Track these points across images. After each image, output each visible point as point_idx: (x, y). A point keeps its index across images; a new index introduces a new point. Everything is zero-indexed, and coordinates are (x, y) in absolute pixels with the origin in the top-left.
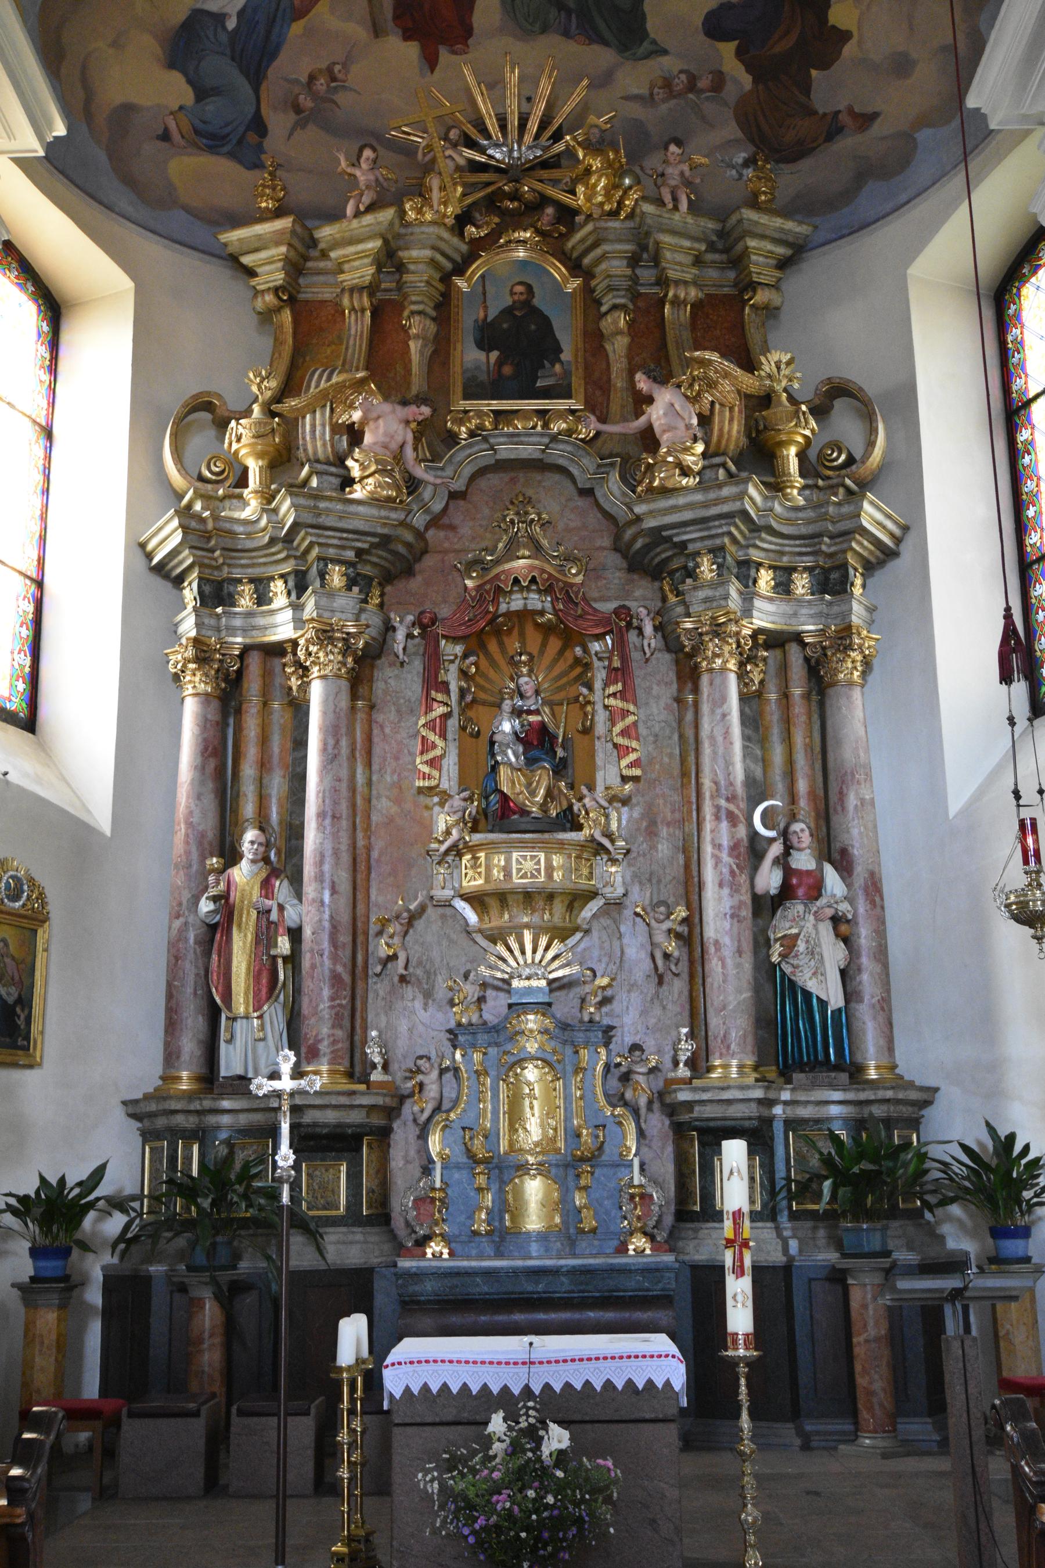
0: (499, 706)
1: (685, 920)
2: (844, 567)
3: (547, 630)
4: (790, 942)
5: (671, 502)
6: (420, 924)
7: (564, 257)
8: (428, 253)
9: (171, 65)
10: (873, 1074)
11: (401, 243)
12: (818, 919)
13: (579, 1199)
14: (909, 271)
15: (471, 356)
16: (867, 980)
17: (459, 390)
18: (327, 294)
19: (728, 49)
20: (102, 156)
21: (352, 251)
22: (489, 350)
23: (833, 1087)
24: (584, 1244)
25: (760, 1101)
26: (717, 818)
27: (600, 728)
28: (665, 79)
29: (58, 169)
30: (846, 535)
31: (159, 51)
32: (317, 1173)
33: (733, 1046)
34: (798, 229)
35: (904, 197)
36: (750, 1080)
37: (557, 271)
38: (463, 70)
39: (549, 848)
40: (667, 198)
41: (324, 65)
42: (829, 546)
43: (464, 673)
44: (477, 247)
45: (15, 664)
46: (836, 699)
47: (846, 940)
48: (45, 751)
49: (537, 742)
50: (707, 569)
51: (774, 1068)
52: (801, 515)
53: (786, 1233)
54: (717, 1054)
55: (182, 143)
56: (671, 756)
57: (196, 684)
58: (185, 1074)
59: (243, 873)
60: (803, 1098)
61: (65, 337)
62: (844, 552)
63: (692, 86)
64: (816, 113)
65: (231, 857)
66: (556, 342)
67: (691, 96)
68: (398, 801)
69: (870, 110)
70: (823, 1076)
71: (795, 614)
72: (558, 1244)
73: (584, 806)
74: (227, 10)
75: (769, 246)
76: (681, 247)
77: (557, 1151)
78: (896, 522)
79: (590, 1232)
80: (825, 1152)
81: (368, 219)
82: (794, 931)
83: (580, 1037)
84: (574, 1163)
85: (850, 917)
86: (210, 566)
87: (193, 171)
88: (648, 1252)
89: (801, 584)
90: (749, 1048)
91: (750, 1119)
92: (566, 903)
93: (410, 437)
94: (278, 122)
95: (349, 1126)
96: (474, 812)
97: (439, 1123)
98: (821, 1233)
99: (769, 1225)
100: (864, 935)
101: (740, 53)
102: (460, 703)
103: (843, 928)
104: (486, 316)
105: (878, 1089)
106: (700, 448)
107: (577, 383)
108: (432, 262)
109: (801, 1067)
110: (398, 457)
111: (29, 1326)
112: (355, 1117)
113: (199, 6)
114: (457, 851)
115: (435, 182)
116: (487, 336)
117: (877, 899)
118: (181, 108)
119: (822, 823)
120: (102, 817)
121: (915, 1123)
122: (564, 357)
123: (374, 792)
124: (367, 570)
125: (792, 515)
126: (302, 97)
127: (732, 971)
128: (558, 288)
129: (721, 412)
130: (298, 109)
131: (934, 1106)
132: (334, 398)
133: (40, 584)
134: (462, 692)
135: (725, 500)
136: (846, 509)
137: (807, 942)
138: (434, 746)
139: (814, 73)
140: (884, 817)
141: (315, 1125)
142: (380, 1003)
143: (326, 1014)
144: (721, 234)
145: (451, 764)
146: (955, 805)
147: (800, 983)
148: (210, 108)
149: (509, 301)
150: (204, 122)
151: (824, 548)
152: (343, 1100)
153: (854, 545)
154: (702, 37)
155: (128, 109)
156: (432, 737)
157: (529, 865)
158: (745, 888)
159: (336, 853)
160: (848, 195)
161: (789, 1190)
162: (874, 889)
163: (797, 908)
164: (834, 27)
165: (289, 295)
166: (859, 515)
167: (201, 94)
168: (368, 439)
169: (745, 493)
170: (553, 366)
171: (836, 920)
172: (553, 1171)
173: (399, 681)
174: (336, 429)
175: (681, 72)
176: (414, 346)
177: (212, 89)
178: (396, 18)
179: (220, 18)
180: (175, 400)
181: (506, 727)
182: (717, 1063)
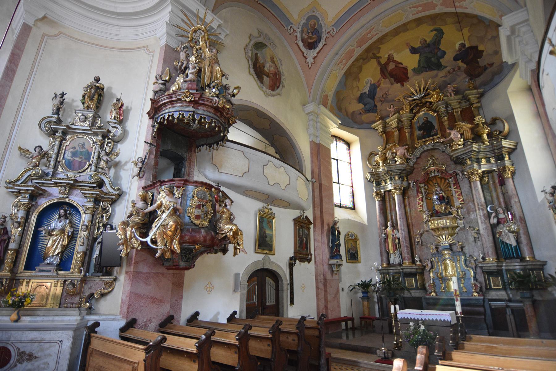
0: (433, 193)
2: (502, 154)
3: (441, 178)
6: (424, 235)
7: (432, 110)
10: (528, 259)
15: (417, 133)
16: (523, 239)
17: (416, 139)
18: (390, 130)
20: (351, 120)
21: (393, 122)
25: (497, 266)
26: (479, 210)
27: (454, 195)
36: (494, 262)
37: (431, 113)
38: (407, 85)
39: (448, 219)
40: (449, 94)
43: (425, 189)
44: (415, 114)
48: (357, 213)
49: (441, 199)
50: (469, 162)
57: (377, 199)
59: (389, 229)
61: (351, 148)
63: (454, 70)
65: (387, 227)
68: (416, 213)
70: (513, 260)
81: (394, 116)
83: (457, 254)
86: (375, 179)
87: (365, 117)
89: (493, 160)
93: (406, 151)
94: (378, 104)
101: (462, 62)
106: (462, 140)
107: (439, 132)
108: (407, 119)
110: (404, 155)
111: (363, 304)
112: (414, 270)
114: (428, 221)
115: (404, 107)
116: (420, 129)
120: (366, 222)
121: (542, 270)
124: (402, 175)
127: (487, 240)
128: (432, 116)
130: (381, 101)
132: (391, 148)
133: (352, 187)
134: (425, 192)
136: (498, 144)
143: (406, 253)
144: (463, 97)
145: (425, 206)
155: (354, 112)
157: (441, 223)
159: (403, 225)
160: (492, 79)
162: (523, 220)
165: (384, 132)
167: (365, 105)
168: (398, 154)
173: (413, 192)
174: (392, 153)
176: (407, 134)
179: (365, 93)
180: (368, 154)
181: (435, 197)
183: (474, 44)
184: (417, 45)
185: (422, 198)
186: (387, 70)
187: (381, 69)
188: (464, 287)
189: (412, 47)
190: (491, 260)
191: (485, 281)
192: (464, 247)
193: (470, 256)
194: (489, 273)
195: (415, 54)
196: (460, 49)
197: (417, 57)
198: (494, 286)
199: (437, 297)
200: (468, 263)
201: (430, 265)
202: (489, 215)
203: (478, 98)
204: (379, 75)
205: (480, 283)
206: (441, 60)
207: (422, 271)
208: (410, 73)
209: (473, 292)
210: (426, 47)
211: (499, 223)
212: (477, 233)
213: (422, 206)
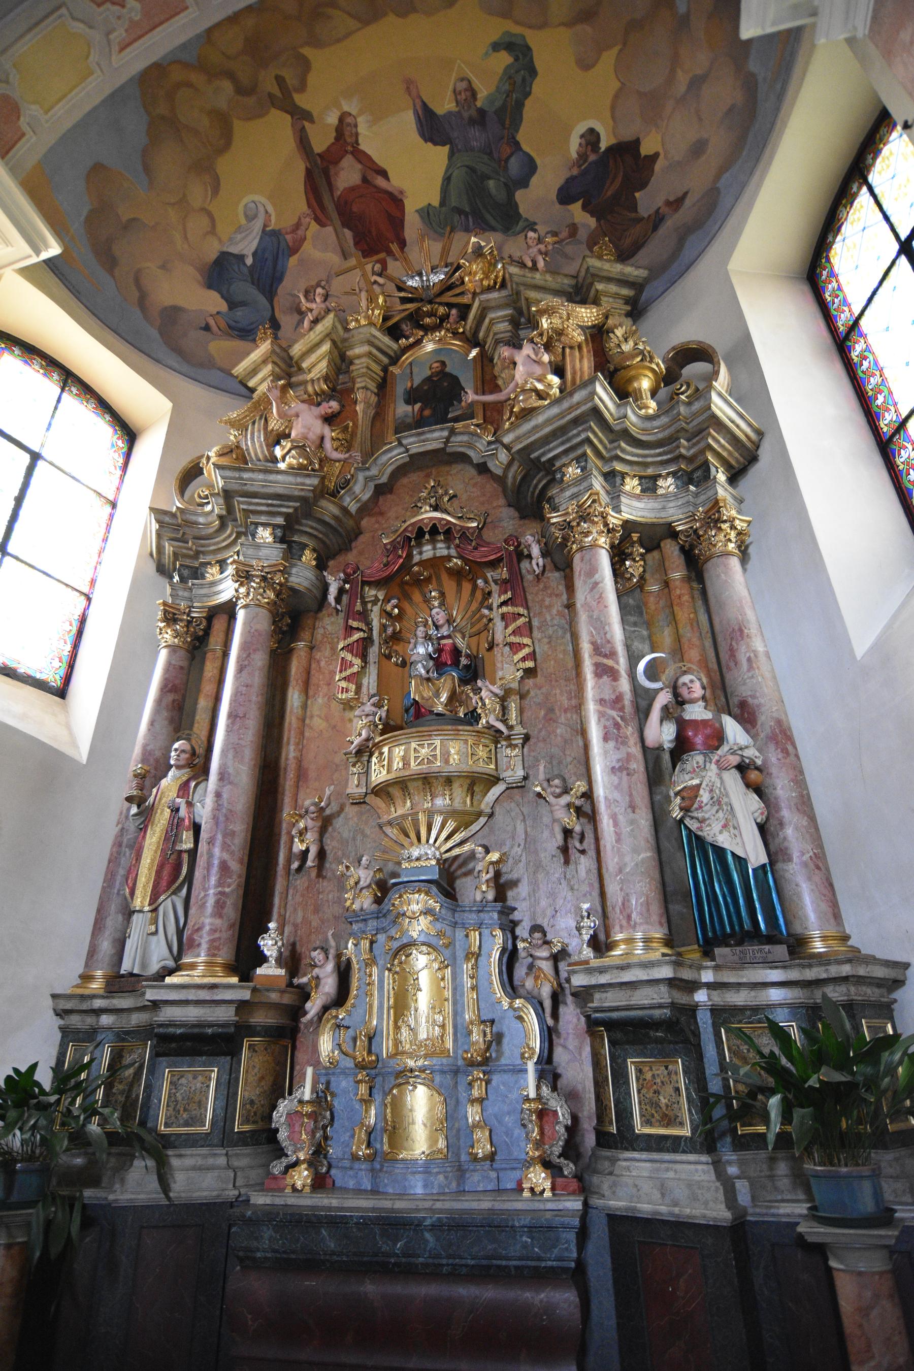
1: (584, 795)
4: (690, 795)
5: (533, 423)
8: (366, 348)
9: (210, 286)
10: (818, 947)
11: (347, 344)
12: (722, 768)
13: (473, 1114)
14: (729, 267)
16: (792, 834)
17: (391, 431)
19: (576, 208)
20: (154, 333)
22: (415, 402)
23: (772, 964)
24: (476, 1177)
25: (672, 983)
29: (57, 276)
30: (699, 433)
31: (200, 278)
32: (183, 1081)
33: (634, 916)
34: (636, 273)
35: (714, 232)
42: (688, 449)
46: (712, 571)
47: (758, 790)
51: (696, 947)
52: (656, 423)
53: (732, 1170)
54: (617, 928)
56: (565, 652)
58: (99, 973)
60: (732, 980)
62: (702, 452)
68: (327, 719)
70: (752, 950)
71: (664, 508)
72: (441, 1177)
73: (481, 698)
74: (245, 252)
77: (444, 1052)
78: (750, 425)
79: (485, 1158)
80: (766, 1051)
82: (695, 782)
84: (470, 1067)
85: (759, 762)
88: (548, 1194)
89: (667, 485)
90: (655, 918)
91: (660, 1006)
92: (466, 787)
95: (211, 1025)
96: (384, 715)
97: (328, 1021)
98: (782, 1168)
99: (705, 1158)
100: (782, 787)
101: (584, 207)
102: (380, 635)
103: (753, 775)
105: (829, 964)
109: (723, 940)
112: (226, 1014)
113: (225, 249)
116: (411, 397)
117: (790, 748)
118: (218, 313)
119: (719, 693)
121: (886, 1010)
123: (308, 713)
125: (648, 425)
127: (626, 829)
129: (571, 355)
131: (905, 988)
134: (384, 627)
135: (578, 404)
136: (696, 406)
137: (711, 791)
139: (637, 195)
140: (777, 659)
141: (171, 1024)
142: (298, 898)
143: (211, 902)
145: (370, 681)
146: (862, 642)
147: (709, 839)
148: (239, 313)
151: (683, 451)
152: (204, 995)
153: (710, 441)
154: (558, 206)
156: (349, 657)
157: (424, 751)
158: (633, 740)
160: (675, 255)
161: (729, 1106)
162: (782, 737)
163: (696, 759)
166: (710, 408)
169: (594, 393)
171: (742, 768)
172: (438, 1078)
179: (241, 258)
181: (421, 650)
182: (619, 937)
183: (627, 135)
184: (444, 105)
185: (367, 642)
187: (309, 174)
188: (483, 1124)
189: (424, 104)
190: (640, 950)
191: (599, 1084)
192: (514, 883)
193: (537, 928)
194: (623, 1034)
195: (435, 144)
196: (582, 156)
198: (647, 1122)
199: (326, 1201)
200: (520, 971)
201: (329, 985)
202: (642, 704)
204: (298, 203)
205: (572, 1097)
206: (519, 195)
207: (287, 1033)
208: (412, 224)
209: (528, 1163)
210: (472, 122)
211: (682, 747)
212: (579, 811)
213: (356, 678)
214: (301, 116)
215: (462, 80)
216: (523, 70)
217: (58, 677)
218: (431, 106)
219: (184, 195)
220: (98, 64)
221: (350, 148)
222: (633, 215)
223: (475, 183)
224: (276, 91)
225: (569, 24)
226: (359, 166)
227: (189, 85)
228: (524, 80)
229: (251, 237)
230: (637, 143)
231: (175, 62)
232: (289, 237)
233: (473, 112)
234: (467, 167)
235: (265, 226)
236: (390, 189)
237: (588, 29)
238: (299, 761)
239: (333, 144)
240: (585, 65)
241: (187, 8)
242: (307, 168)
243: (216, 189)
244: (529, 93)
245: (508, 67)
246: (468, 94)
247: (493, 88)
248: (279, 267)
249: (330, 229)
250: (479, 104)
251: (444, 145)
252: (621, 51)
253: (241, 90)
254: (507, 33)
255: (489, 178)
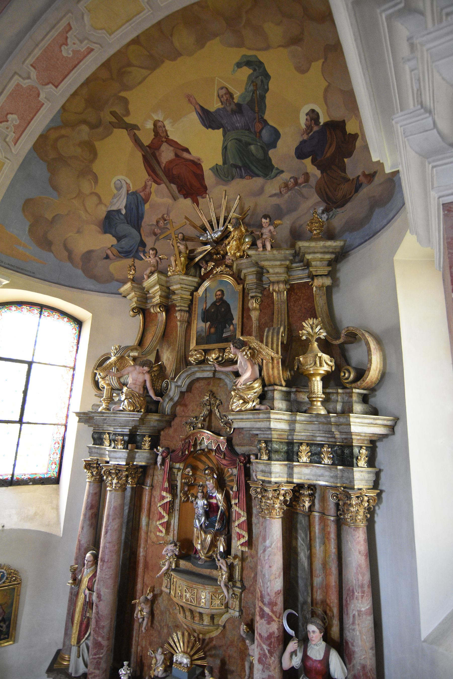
9: (105, 232)
14: (395, 258)
15: (199, 325)
19: (308, 161)
20: (80, 272)
28: (285, 183)
31: (99, 229)
35: (391, 215)
41: (160, 216)
45: (51, 459)
55: (115, 258)
63: (296, 183)
64: (349, 180)
66: (232, 315)
67: (296, 187)
69: (372, 171)
74: (120, 207)
75: (319, 256)
76: (276, 265)
94: (149, 241)
101: (313, 162)
104: (206, 307)
113: (109, 209)
116: (206, 316)
118: (112, 246)
122: (234, 322)
126: (156, 230)
130: (155, 234)
138: (163, 517)
139: (346, 160)
148: (123, 243)
149: (215, 299)
150: (122, 248)
155: (90, 252)
160: (367, 218)
164: (350, 134)
167: (119, 239)
170: (230, 327)
175: (290, 178)
177: (123, 236)
178: (179, 191)
179: (119, 211)
183: (337, 116)
184: (214, 105)
186: (159, 163)
187: (145, 158)
189: (202, 107)
195: (213, 129)
196: (309, 128)
197: (217, 135)
203: (330, 263)
204: (143, 175)
206: (271, 153)
208: (209, 178)
210: (233, 112)
214: (131, 128)
215: (222, 88)
216: (260, 77)
217: (55, 473)
218: (206, 107)
219: (80, 190)
220: (6, 158)
221: (164, 139)
222: (343, 174)
223: (243, 148)
224: (114, 120)
225: (285, 46)
226: (171, 148)
227: (62, 136)
228: (262, 81)
229: (121, 199)
230: (343, 123)
231: (50, 129)
232: (142, 194)
233: (233, 106)
234: (236, 139)
235: (128, 191)
236: (192, 158)
237: (299, 49)
238: (145, 557)
239: (154, 139)
240: (303, 70)
241: (43, 104)
242: (143, 155)
243: (96, 179)
244: (268, 89)
245: (250, 76)
246: (228, 96)
247: (243, 90)
248: (140, 212)
249: (163, 186)
250: (236, 101)
251: (218, 128)
252: (324, 62)
253: (93, 127)
254: (244, 56)
255: (250, 144)
